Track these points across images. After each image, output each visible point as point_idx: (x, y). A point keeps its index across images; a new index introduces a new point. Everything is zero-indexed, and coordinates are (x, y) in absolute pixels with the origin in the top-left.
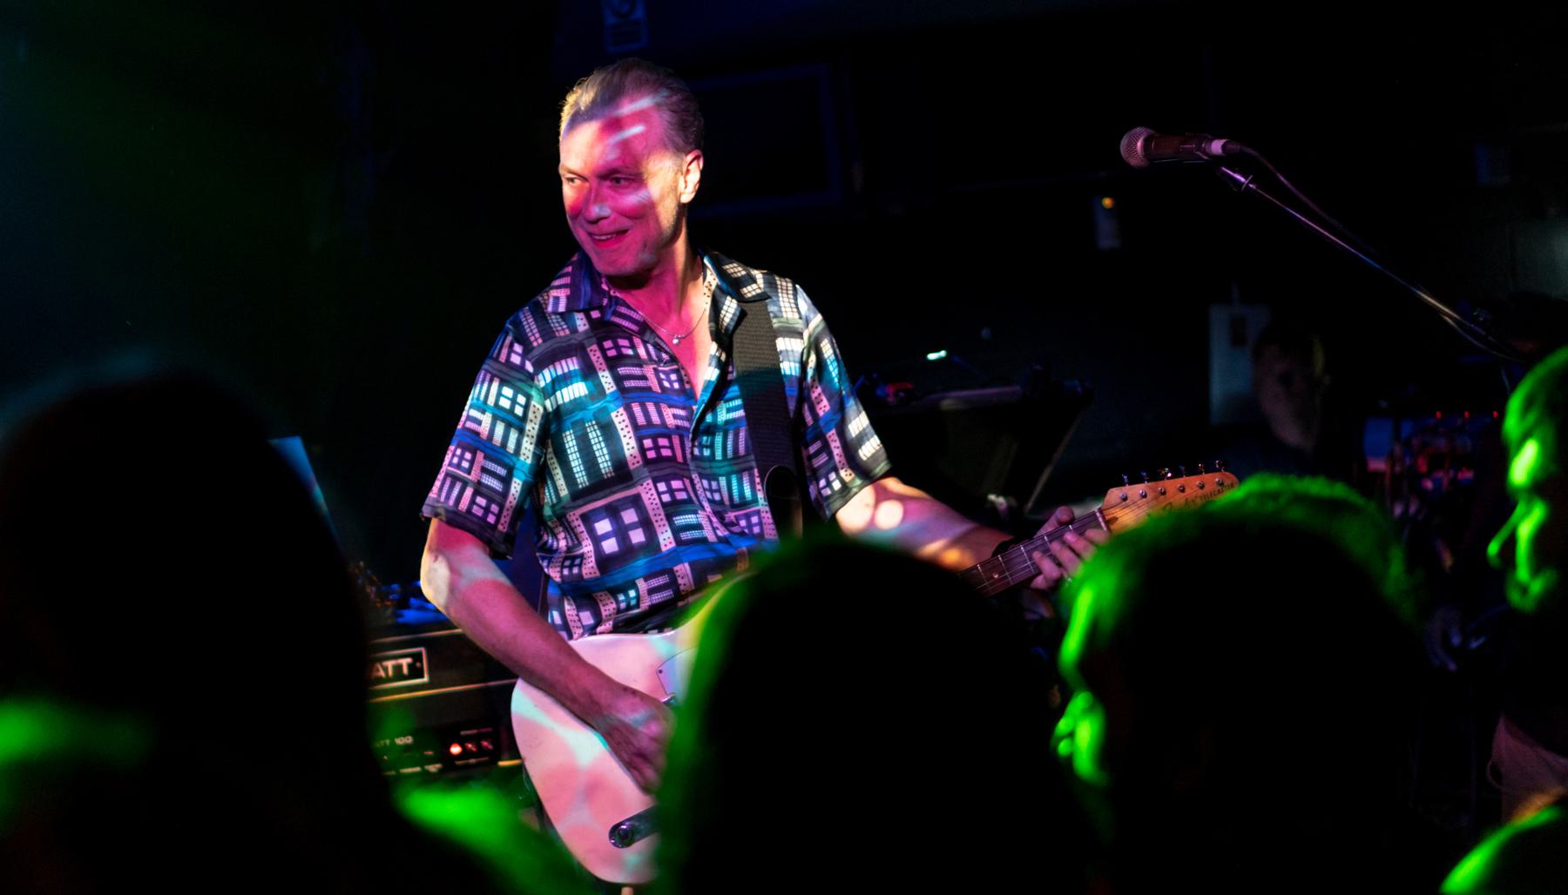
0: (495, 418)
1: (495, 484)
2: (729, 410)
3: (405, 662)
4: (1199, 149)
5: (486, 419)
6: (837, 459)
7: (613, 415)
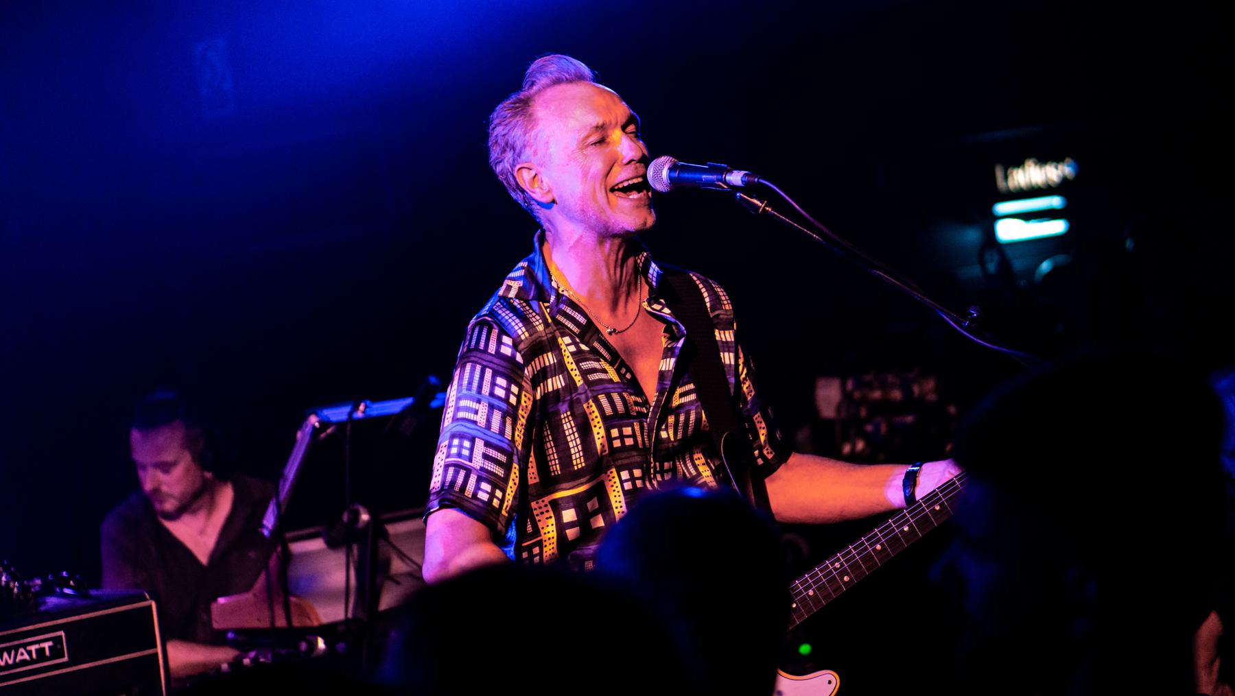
0: (492, 407)
1: (500, 472)
2: (682, 395)
3: (46, 645)
5: (483, 409)
6: (762, 438)
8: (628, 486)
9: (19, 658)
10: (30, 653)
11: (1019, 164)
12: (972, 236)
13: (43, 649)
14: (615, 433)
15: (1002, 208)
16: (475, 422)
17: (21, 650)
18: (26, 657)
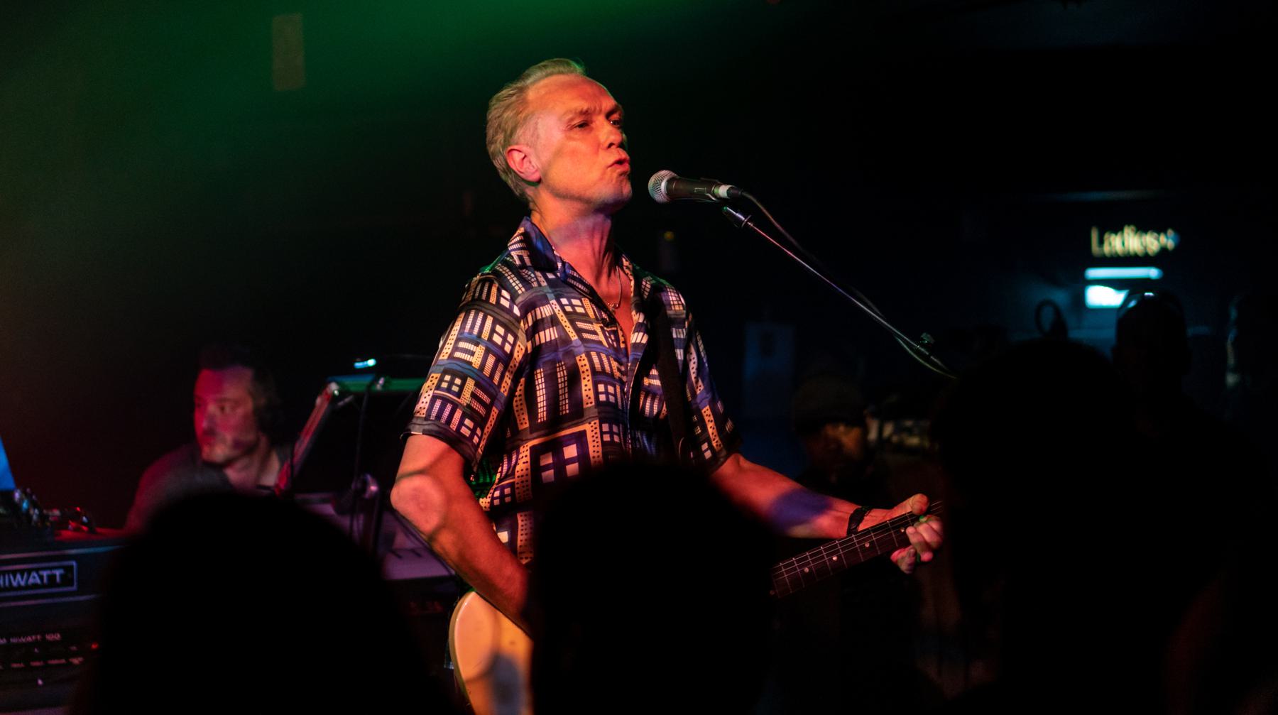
0: (488, 352)
1: (482, 410)
3: (58, 573)
5: (480, 351)
6: (710, 431)
8: (607, 438)
9: (31, 581)
10: (41, 578)
11: (1117, 229)
12: (1060, 297)
13: (54, 576)
14: (601, 388)
15: (1093, 273)
16: (470, 363)
17: (34, 574)
18: (38, 581)
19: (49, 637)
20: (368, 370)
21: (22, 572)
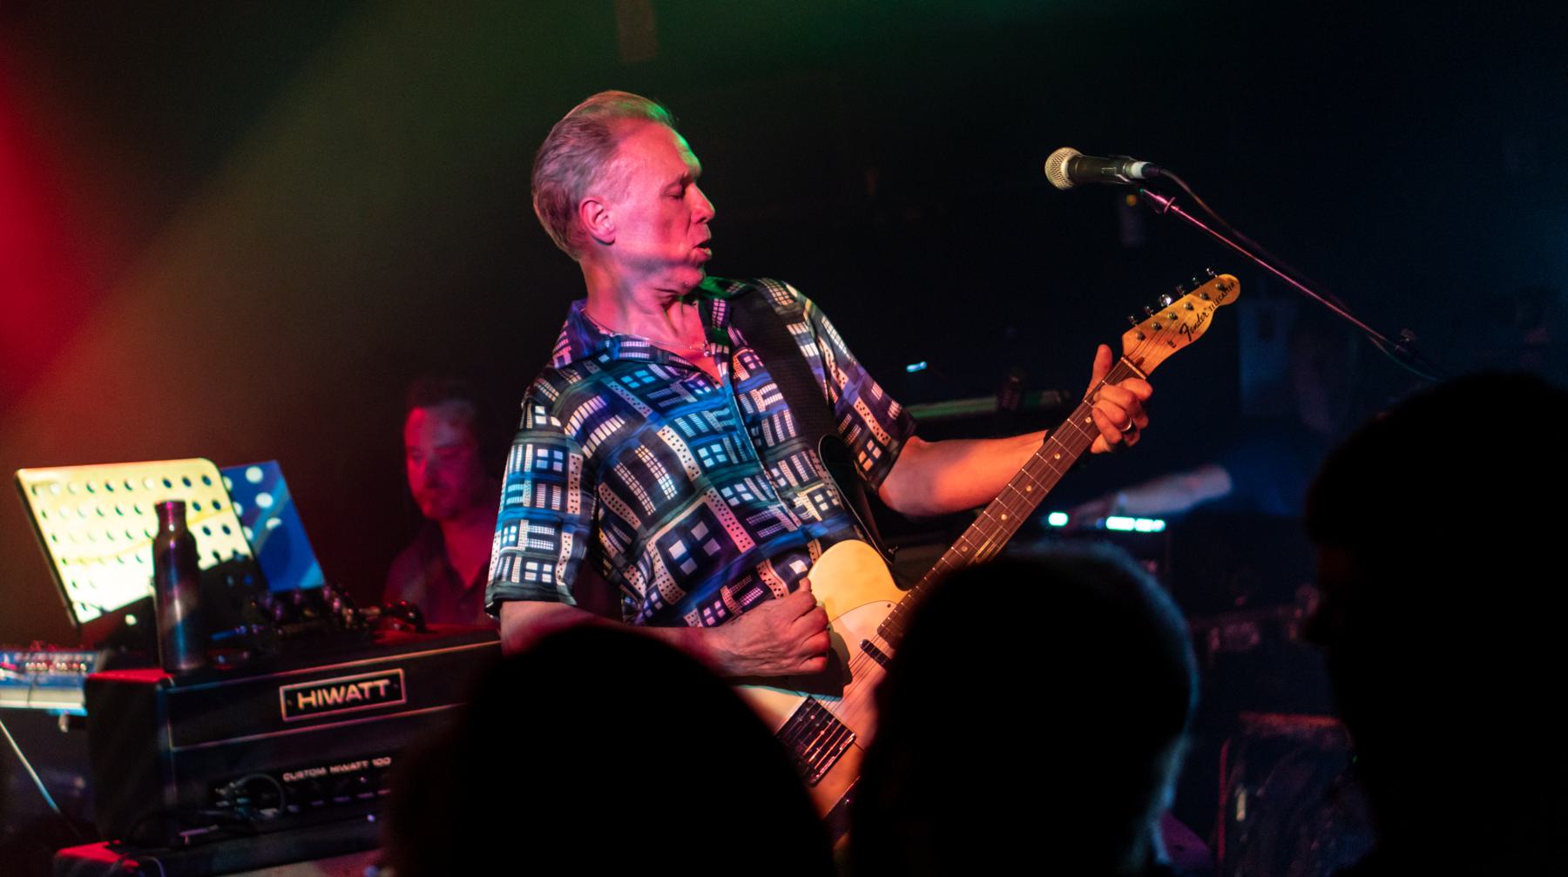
1: (548, 546)
3: (381, 683)
4: (1120, 172)
7: (660, 434)
9: (350, 696)
14: (703, 452)
16: (521, 505)
18: (358, 696)
19: (378, 763)
20: (223, 808)
21: (338, 686)
